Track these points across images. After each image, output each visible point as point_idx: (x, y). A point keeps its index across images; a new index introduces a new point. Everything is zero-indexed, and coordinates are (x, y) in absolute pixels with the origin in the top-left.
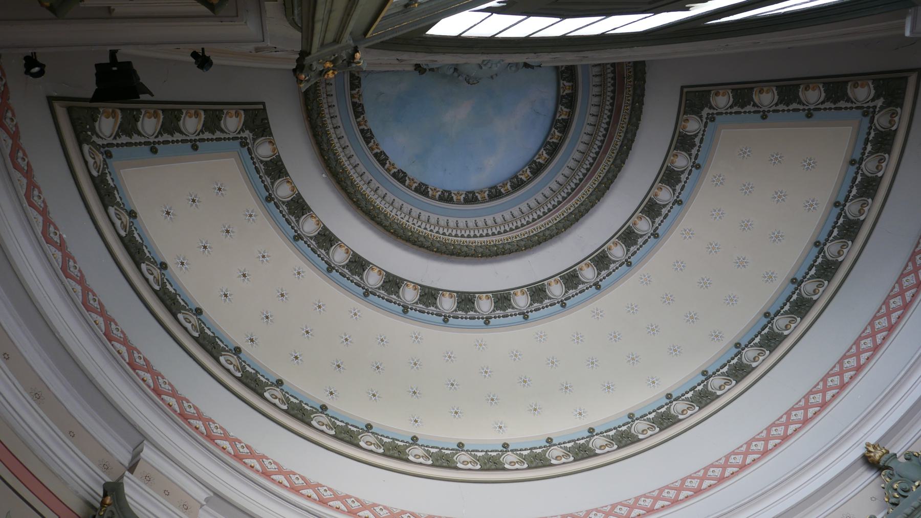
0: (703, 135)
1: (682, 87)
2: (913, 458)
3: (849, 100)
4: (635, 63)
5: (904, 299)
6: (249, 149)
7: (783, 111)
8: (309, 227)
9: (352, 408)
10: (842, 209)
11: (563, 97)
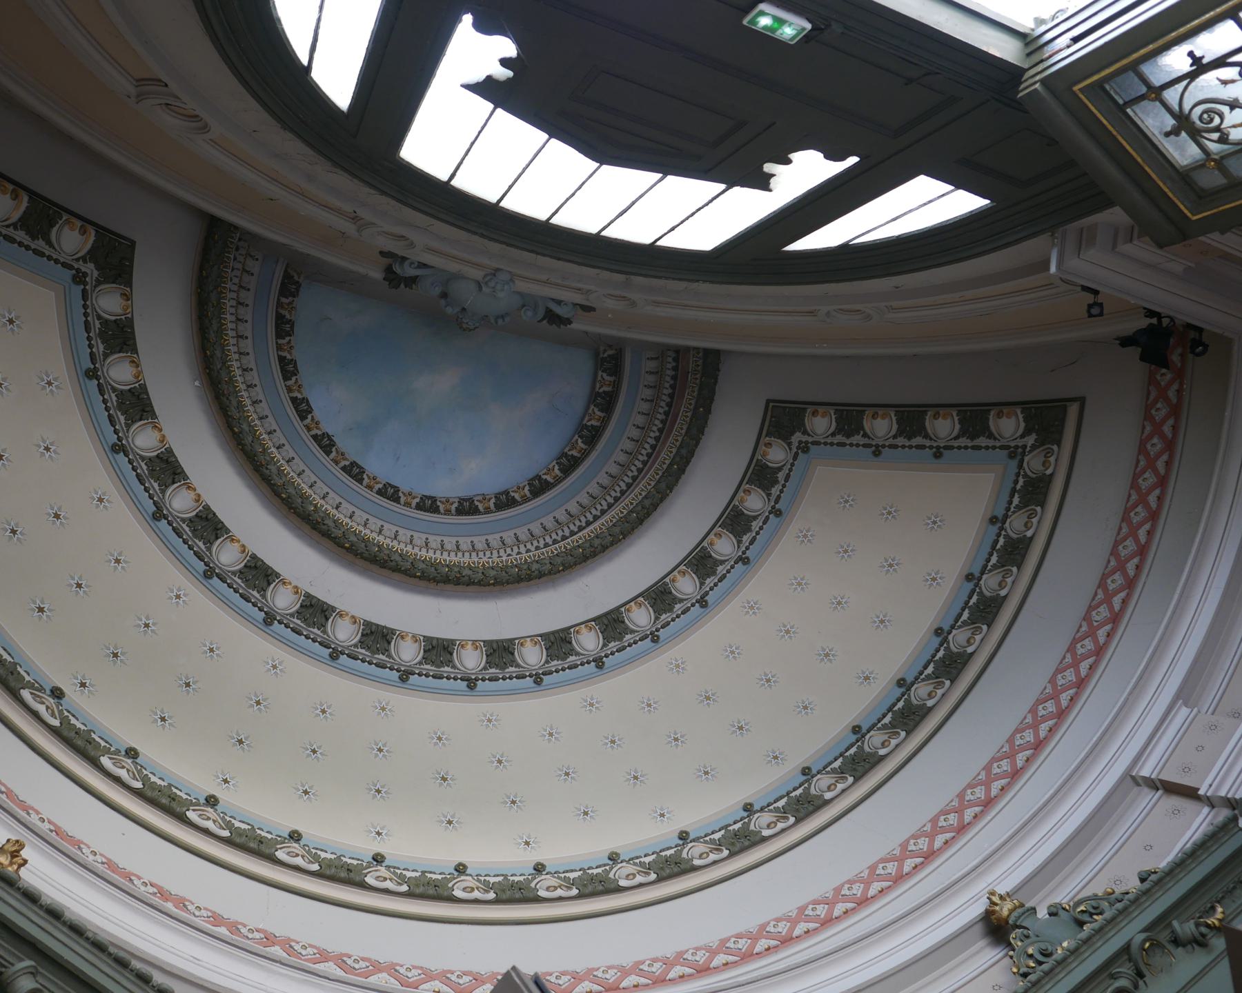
0: (790, 470)
1: (768, 401)
2: (1061, 912)
3: (991, 436)
4: (707, 352)
5: (1058, 703)
6: (84, 292)
7: (903, 447)
8: (144, 440)
9: (111, 719)
10: (977, 585)
11: (598, 394)
